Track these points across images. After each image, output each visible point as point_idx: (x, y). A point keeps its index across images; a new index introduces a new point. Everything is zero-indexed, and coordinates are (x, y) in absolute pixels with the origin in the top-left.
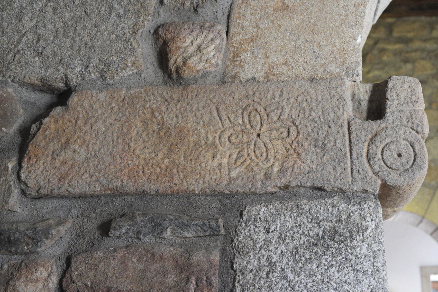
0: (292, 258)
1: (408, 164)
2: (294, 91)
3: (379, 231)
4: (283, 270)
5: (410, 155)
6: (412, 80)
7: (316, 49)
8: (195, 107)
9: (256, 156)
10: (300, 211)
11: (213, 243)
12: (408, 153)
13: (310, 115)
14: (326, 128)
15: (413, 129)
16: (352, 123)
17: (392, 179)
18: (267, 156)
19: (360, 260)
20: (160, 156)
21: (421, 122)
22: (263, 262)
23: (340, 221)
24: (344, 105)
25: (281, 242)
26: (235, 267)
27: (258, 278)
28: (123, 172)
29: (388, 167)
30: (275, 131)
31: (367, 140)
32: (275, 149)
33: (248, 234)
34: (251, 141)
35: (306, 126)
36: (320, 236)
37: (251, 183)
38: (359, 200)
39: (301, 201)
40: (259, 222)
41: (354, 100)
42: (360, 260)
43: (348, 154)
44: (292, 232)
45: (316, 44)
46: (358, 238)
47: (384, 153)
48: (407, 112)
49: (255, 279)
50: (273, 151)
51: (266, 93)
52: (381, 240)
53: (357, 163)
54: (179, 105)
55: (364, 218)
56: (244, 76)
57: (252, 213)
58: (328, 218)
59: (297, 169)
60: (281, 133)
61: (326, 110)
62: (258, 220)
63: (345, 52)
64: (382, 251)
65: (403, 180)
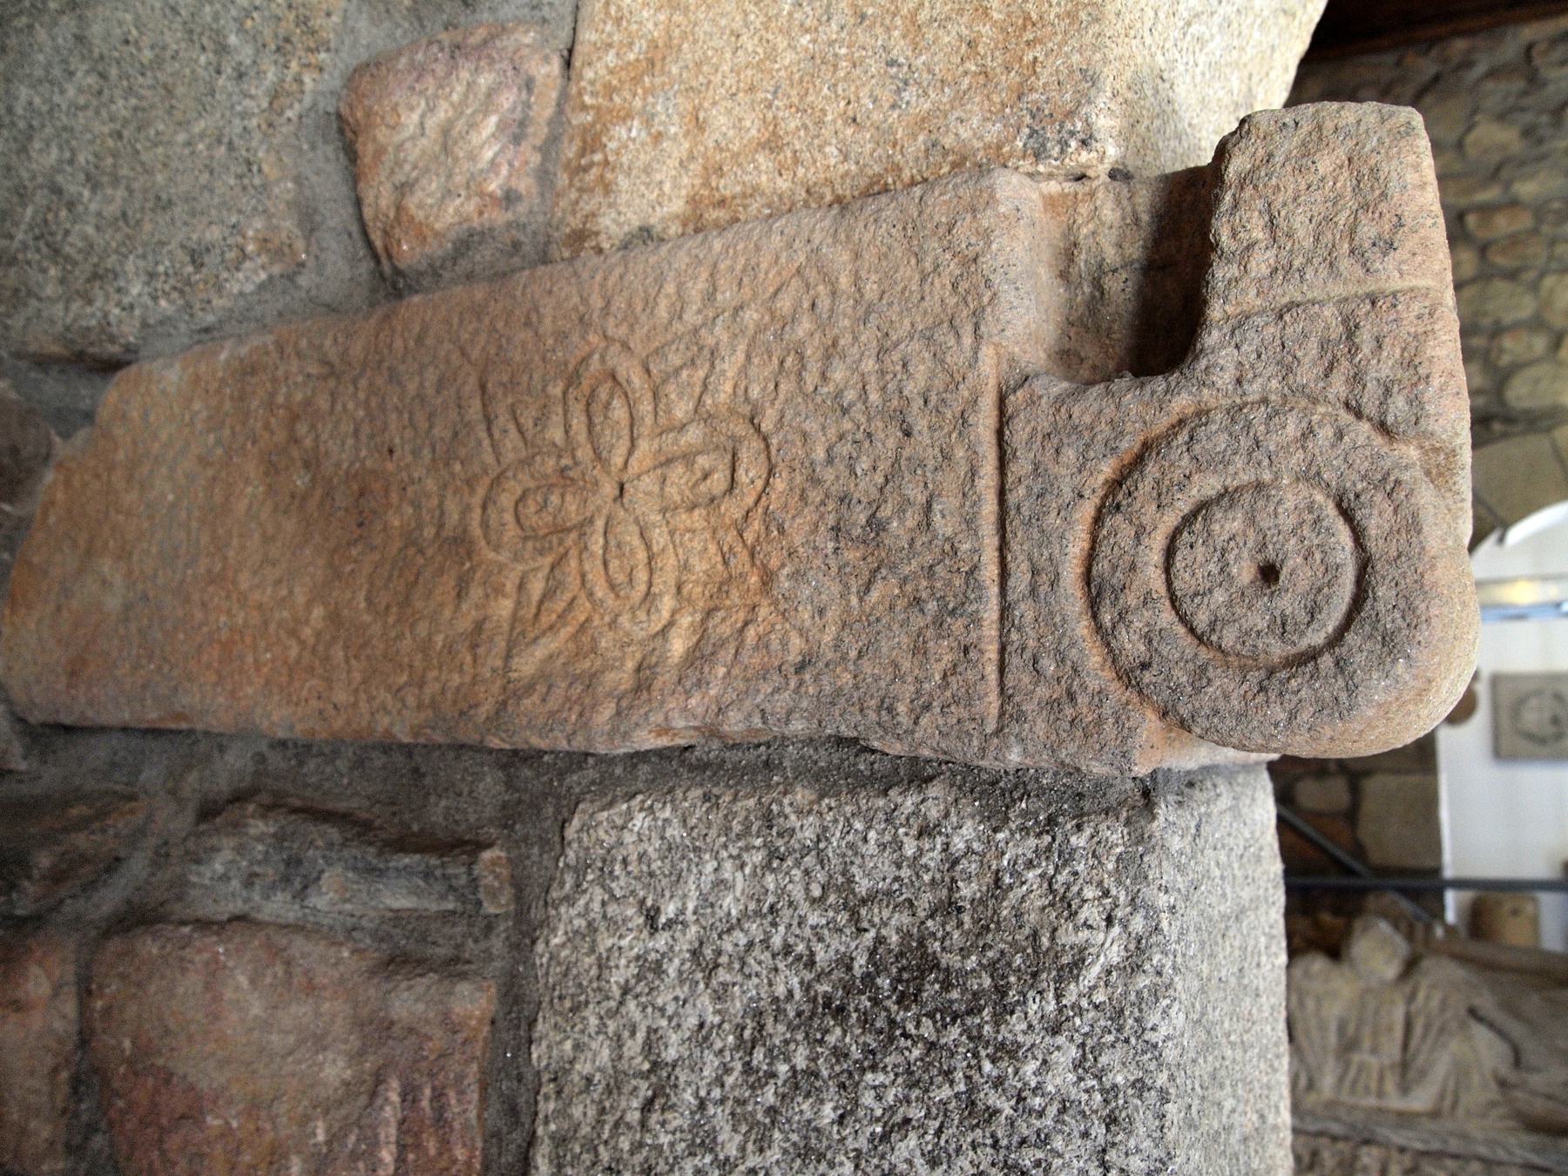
0: (737, 1056)
1: (1315, 625)
2: (764, 266)
3: (1142, 981)
4: (702, 1105)
5: (1332, 571)
6: (1373, 119)
7: (901, 49)
8: (412, 387)
9: (612, 586)
10: (780, 842)
11: (476, 941)
12: (1318, 556)
13: (824, 377)
14: (889, 439)
15: (1359, 415)
16: (1016, 399)
17: (1216, 712)
18: (650, 585)
19: (1038, 1123)
20: (300, 598)
21: (1410, 364)
22: (632, 1053)
23: (949, 908)
24: (984, 310)
25: (699, 975)
26: (535, 1056)
27: (610, 1119)
28: (205, 658)
29: (1200, 639)
30: (680, 470)
31: (1087, 493)
32: (680, 551)
33: (584, 923)
34: (591, 521)
35: (805, 436)
36: (858, 971)
37: (577, 708)
38: (1052, 809)
39: (785, 793)
40: (623, 878)
41: (1074, 271)
42: (1038, 1123)
43: (990, 572)
44: (743, 941)
45: (898, 21)
46: (1035, 1007)
47: (1179, 563)
48: (1328, 312)
49: (600, 1122)
50: (672, 561)
51: (653, 292)
52: (1148, 1036)
53: (1030, 616)
54: (363, 383)
55: (1070, 906)
56: (614, 228)
57: (593, 838)
58: (896, 886)
59: (756, 648)
60: (706, 477)
61: (896, 345)
62: (618, 869)
63: (1029, 36)
64: (1153, 1093)
65: (1283, 716)
